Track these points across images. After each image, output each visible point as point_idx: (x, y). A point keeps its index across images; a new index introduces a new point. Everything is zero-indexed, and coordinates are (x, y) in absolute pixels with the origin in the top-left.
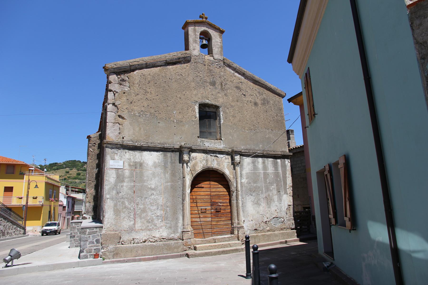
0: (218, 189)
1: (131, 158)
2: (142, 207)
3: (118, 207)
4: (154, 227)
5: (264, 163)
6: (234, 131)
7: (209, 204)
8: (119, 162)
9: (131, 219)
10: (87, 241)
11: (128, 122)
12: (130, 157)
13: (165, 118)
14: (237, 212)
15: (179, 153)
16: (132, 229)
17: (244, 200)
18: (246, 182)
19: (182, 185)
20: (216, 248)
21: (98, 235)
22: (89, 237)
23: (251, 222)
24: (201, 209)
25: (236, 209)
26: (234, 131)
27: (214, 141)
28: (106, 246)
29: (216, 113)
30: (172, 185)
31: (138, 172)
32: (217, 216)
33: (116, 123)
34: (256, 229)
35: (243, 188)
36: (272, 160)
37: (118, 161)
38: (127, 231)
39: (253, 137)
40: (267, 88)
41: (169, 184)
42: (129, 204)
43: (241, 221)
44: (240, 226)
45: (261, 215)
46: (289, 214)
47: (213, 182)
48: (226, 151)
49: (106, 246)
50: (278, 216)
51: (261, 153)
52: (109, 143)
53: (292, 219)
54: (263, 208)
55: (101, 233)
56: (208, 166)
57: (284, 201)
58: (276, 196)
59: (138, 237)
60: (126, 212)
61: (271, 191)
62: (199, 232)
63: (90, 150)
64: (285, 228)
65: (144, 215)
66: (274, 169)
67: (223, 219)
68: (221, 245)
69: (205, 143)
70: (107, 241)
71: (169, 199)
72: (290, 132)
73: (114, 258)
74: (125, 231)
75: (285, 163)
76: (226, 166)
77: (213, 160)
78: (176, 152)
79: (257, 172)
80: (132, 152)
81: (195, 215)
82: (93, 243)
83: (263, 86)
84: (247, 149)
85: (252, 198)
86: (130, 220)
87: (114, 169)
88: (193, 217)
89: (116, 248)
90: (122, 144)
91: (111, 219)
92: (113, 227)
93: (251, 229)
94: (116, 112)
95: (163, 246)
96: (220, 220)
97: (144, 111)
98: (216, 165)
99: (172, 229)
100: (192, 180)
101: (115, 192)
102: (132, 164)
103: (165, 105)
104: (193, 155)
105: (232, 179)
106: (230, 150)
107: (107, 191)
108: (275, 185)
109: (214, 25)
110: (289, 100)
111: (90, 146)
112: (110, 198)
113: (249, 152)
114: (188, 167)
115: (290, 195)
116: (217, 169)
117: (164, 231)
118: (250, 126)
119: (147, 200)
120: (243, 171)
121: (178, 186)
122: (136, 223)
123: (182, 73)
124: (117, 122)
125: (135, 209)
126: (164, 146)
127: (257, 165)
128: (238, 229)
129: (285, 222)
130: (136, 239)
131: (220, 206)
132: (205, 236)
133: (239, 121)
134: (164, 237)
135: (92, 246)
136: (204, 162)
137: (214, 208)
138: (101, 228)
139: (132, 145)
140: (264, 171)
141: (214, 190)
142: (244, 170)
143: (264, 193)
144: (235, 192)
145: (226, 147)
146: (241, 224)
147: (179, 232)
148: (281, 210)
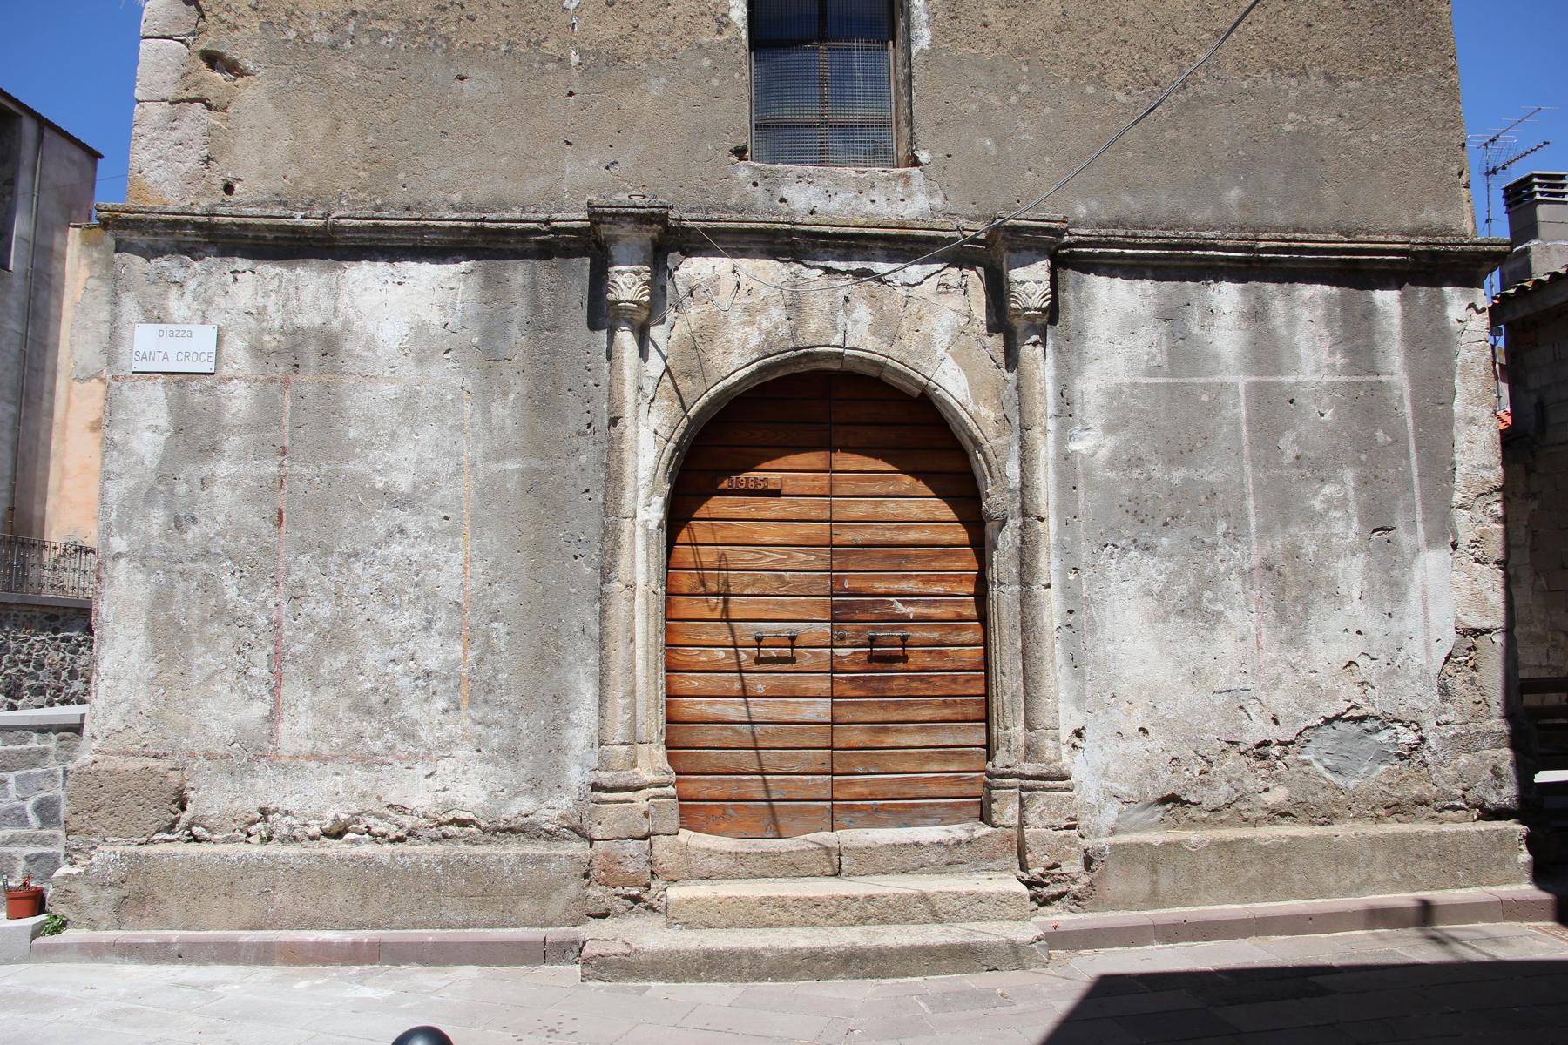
0: (892, 508)
1: (265, 307)
2: (325, 611)
3: (178, 610)
4: (400, 747)
5: (1256, 315)
6: (1014, 100)
7: (818, 607)
8: (190, 334)
9: (253, 689)
11: (259, 88)
12: (261, 301)
13: (503, 48)
14: (1024, 665)
15: (588, 261)
16: (259, 748)
17: (1084, 582)
18: (1103, 454)
19: (602, 475)
20: (813, 919)
21: (51, 775)
23: (1137, 746)
24: (759, 639)
25: (1019, 644)
26: (1014, 100)
27: (854, 174)
30: (535, 472)
31: (310, 390)
32: (875, 690)
33: (192, 101)
34: (1173, 799)
35: (1082, 495)
36: (1327, 298)
37: (187, 327)
38: (224, 762)
39: (1170, 134)
41: (510, 466)
42: (246, 591)
43: (1046, 736)
44: (1041, 768)
46: (1465, 697)
47: (856, 457)
48: (942, 234)
49: (86, 847)
50: (1370, 710)
51: (1230, 243)
52: (127, 220)
53: (1490, 733)
54: (1243, 644)
55: (70, 766)
56: (800, 341)
58: (1359, 561)
59: (291, 804)
60: (227, 643)
61: (1311, 518)
62: (734, 793)
64: (1426, 803)
65: (335, 663)
66: (1339, 360)
67: (926, 714)
68: (855, 899)
69: (785, 191)
70: (96, 814)
71: (505, 564)
72: (1536, 188)
73: (120, 924)
74: (210, 757)
75: (1443, 316)
76: (947, 339)
77: (846, 299)
78: (567, 253)
79: (1195, 380)
80: (278, 270)
81: (707, 680)
82: (22, 820)
84: (1117, 223)
85: (1152, 569)
86: (244, 691)
87: (162, 379)
88: (697, 689)
90: (205, 219)
91: (131, 683)
92: (140, 730)
93: (1136, 794)
94: (189, 35)
95: (439, 870)
97: (364, 14)
98: (866, 334)
99: (523, 761)
100: (676, 438)
101: (158, 516)
102: (275, 343)
104: (692, 269)
105: (990, 431)
106: (980, 226)
107: (114, 514)
108: (1349, 476)
112: (130, 556)
113: (1134, 236)
114: (653, 354)
115: (1478, 552)
116: (873, 363)
117: (464, 772)
118: (1148, 60)
119: (359, 571)
120: (1080, 374)
121: (572, 482)
122: (286, 714)
124: (192, 94)
125: (277, 624)
126: (483, 220)
127: (1196, 330)
128: (1023, 788)
129: (1429, 758)
130: (277, 811)
131: (905, 618)
132: (782, 821)
133: (1059, 30)
134: (464, 816)
136: (777, 313)
137: (858, 632)
138: (68, 734)
139: (269, 228)
140: (1253, 379)
141: (859, 509)
142: (1092, 370)
143: (1253, 538)
144: (1014, 522)
145: (950, 207)
146: (1049, 754)
148: (1394, 666)
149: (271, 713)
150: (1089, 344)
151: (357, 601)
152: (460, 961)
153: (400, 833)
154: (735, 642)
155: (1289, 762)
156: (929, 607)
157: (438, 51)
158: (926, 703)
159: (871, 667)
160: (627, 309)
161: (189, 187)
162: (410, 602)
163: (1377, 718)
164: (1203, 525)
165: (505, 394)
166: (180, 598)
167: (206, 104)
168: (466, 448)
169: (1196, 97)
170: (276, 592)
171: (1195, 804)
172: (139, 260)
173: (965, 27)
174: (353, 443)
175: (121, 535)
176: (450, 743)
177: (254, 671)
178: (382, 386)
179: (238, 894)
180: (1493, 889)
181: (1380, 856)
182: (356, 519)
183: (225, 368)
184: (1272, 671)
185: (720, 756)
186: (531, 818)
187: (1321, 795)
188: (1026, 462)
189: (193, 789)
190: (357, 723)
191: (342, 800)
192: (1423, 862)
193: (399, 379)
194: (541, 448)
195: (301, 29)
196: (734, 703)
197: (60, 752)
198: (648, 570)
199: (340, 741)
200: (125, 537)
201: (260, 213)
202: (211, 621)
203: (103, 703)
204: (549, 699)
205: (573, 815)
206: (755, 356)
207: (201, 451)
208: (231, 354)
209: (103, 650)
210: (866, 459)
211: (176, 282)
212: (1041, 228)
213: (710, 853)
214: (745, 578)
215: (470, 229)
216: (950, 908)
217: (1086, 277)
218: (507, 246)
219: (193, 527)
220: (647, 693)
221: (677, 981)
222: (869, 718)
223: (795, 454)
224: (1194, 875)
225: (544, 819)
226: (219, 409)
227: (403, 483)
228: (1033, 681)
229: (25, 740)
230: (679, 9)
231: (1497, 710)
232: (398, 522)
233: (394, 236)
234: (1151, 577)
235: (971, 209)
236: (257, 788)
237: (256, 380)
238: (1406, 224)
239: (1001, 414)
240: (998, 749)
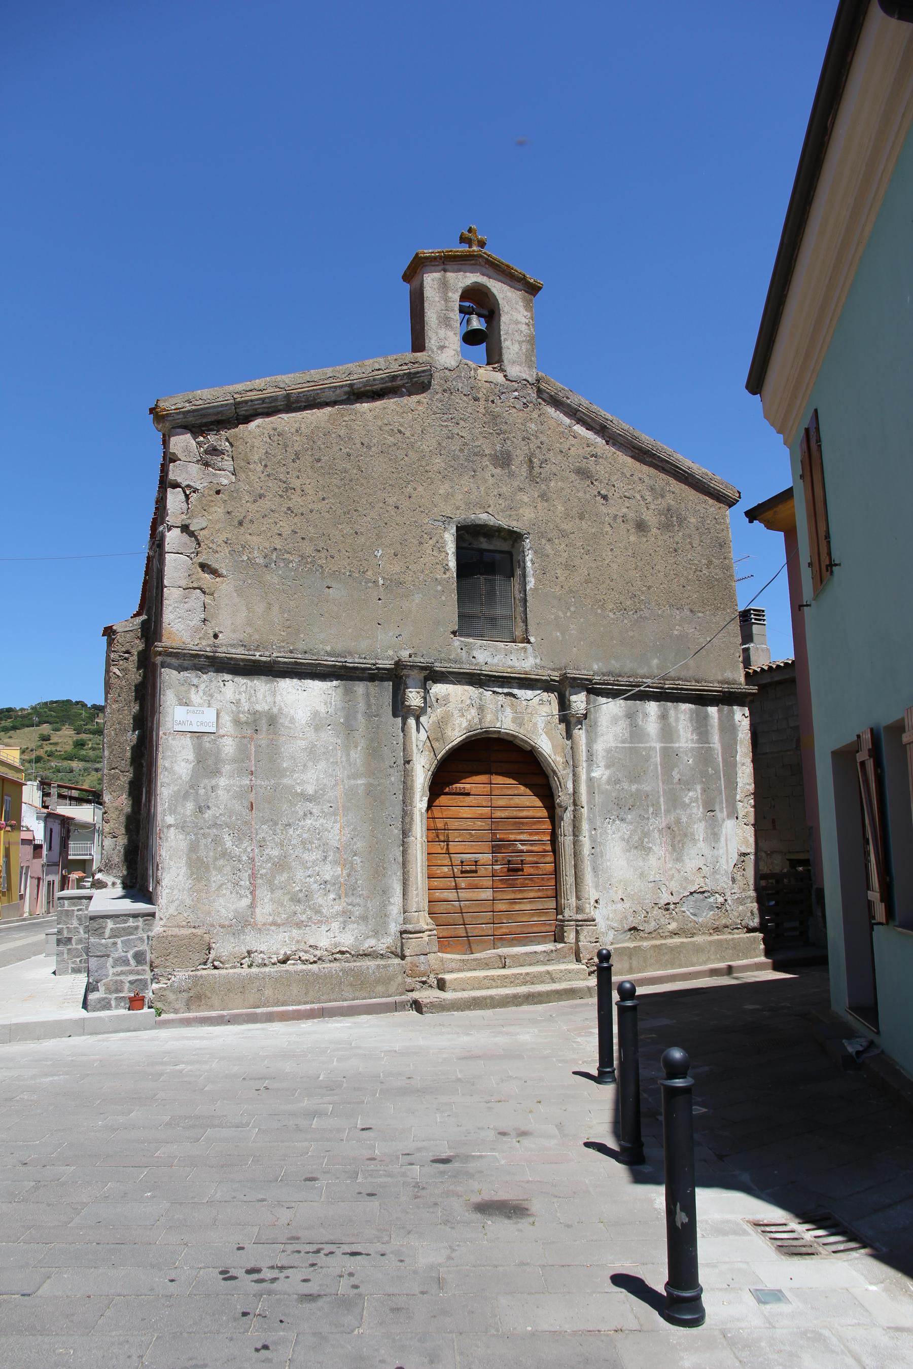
0: (517, 801)
1: (240, 700)
2: (276, 852)
3: (202, 853)
5: (664, 717)
6: (568, 614)
8: (203, 713)
10: (108, 956)
12: (237, 697)
14: (575, 872)
15: (391, 683)
16: (247, 921)
18: (605, 777)
19: (402, 787)
20: (505, 984)
21: (141, 939)
22: (115, 944)
23: (620, 906)
24: (462, 862)
26: (568, 614)
29: (510, 554)
30: (371, 785)
31: (263, 743)
32: (510, 884)
33: (195, 588)
34: (634, 929)
40: (680, 476)
41: (360, 782)
42: (236, 843)
45: (652, 884)
46: (740, 882)
51: (655, 685)
52: (171, 653)
53: (750, 897)
54: (660, 861)
55: (150, 934)
56: (483, 725)
57: (726, 841)
58: (702, 825)
59: (263, 947)
61: (685, 806)
62: (453, 934)
63: (114, 673)
65: (281, 878)
66: (695, 737)
67: (531, 895)
68: (521, 974)
69: (475, 653)
70: (168, 957)
71: (359, 829)
72: (752, 616)
73: (189, 1010)
74: (222, 927)
77: (502, 706)
78: (382, 679)
79: (640, 745)
80: (245, 681)
82: (126, 962)
83: (667, 467)
84: (609, 674)
85: (625, 829)
87: (189, 735)
88: (436, 886)
89: (196, 980)
90: (212, 654)
91: (179, 890)
92: (185, 915)
94: (192, 553)
95: (341, 974)
96: (521, 897)
97: (280, 550)
98: (510, 722)
99: (370, 922)
100: (432, 769)
101: (190, 806)
104: (438, 689)
105: (560, 767)
107: (167, 804)
108: (699, 788)
109: (508, 266)
110: (752, 515)
111: (113, 661)
112: (176, 826)
113: (618, 681)
116: (513, 736)
118: (622, 598)
121: (388, 790)
124: (195, 585)
125: (253, 859)
126: (345, 662)
127: (640, 723)
128: (577, 926)
130: (256, 951)
131: (522, 851)
132: (473, 946)
133: (587, 582)
134: (344, 949)
135: (122, 973)
139: (243, 660)
140: (662, 745)
141: (502, 802)
144: (571, 808)
145: (543, 664)
146: (587, 910)
149: (251, 904)
150: (599, 728)
151: (291, 847)
152: (360, 1014)
153: (315, 959)
154: (452, 863)
155: (677, 912)
156: (532, 846)
157: (317, 573)
158: (531, 890)
159: (509, 874)
160: (414, 709)
161: (195, 634)
162: (316, 848)
163: (709, 892)
164: (644, 809)
165: (356, 747)
166: (203, 847)
167: (202, 591)
168: (339, 773)
169: (641, 617)
170: (251, 844)
171: (642, 931)
172: (175, 672)
173: (548, 578)
174: (286, 770)
177: (242, 883)
178: (299, 742)
179: (247, 992)
180: (752, 960)
181: (713, 948)
182: (289, 807)
183: (221, 730)
184: (670, 873)
185: (446, 917)
186: (374, 948)
187: (689, 925)
188: (575, 782)
189: (214, 943)
190: (293, 907)
191: (288, 944)
192: (728, 950)
193: (306, 739)
194: (374, 774)
195: (249, 555)
196: (452, 892)
197: (145, 927)
198: (422, 831)
199: (285, 916)
200: (173, 816)
202: (220, 859)
203: (166, 901)
204: (381, 892)
205: (392, 946)
206: (465, 732)
207: (211, 772)
208: (224, 723)
210: (505, 778)
211: (194, 685)
212: (584, 678)
213: (452, 960)
214: (456, 834)
215: (340, 666)
216: (558, 976)
217: (598, 698)
218: (355, 675)
220: (423, 888)
221: (462, 1011)
222: (508, 898)
223: (476, 775)
224: (645, 961)
225: (380, 948)
226: (219, 751)
227: (310, 790)
228: (580, 878)
230: (427, 560)
231: (752, 887)
232: (309, 808)
233: (303, 667)
234: (624, 832)
235: (551, 665)
236: (247, 941)
237: (237, 737)
238: (720, 678)
239: (565, 760)
240: (564, 909)
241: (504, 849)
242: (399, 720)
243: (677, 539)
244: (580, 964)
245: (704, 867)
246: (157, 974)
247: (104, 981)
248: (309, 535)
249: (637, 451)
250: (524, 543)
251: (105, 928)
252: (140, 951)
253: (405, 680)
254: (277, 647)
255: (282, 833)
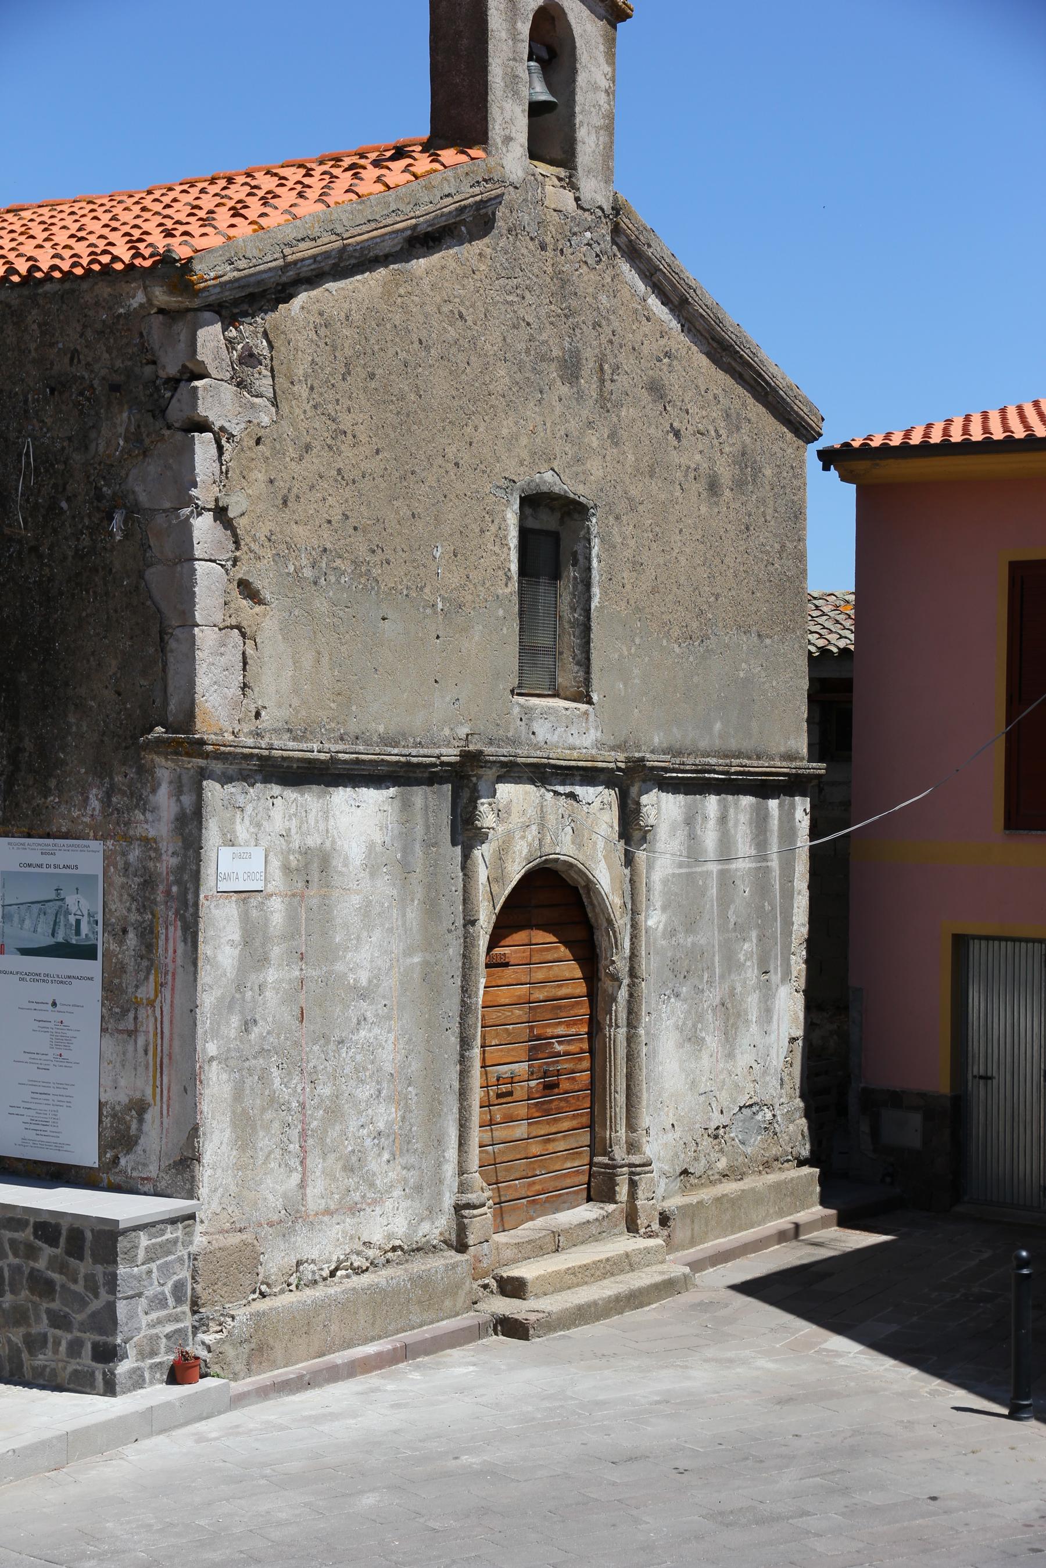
3: (248, 1102)
4: (368, 1195)
7: (521, 1050)
10: (139, 1295)
19: (460, 964)
22: (149, 1272)
23: (670, 1136)
26: (633, 651)
28: (216, 1311)
31: (314, 902)
32: (545, 1110)
33: (232, 627)
40: (760, 390)
45: (702, 1098)
57: (779, 1020)
59: (314, 1254)
70: (216, 1286)
74: (271, 1224)
82: (162, 1303)
83: (748, 374)
85: (679, 1007)
87: (235, 897)
93: (671, 1171)
94: (227, 560)
96: (554, 1130)
99: (425, 1195)
103: (405, 512)
107: (208, 1022)
110: (823, 455)
123: (462, 303)
135: (159, 1322)
144: (626, 981)
147: (447, 1210)
165: (413, 901)
175: (213, 1040)
176: (391, 1187)
179: (312, 1331)
200: (215, 1042)
201: (296, 747)
203: (207, 1189)
209: (207, 1143)
219: (255, 1028)
222: (542, 1133)
229: (163, 1232)
240: (611, 1147)
241: (542, 1052)
242: (458, 849)
243: (750, 507)
244: (637, 1235)
245: (755, 1065)
246: (208, 1318)
247: (135, 1339)
248: (362, 523)
249: (715, 345)
250: (589, 523)
251: (137, 1247)
252: (180, 1280)
253: (475, 784)
254: (326, 730)
255: (334, 1056)
